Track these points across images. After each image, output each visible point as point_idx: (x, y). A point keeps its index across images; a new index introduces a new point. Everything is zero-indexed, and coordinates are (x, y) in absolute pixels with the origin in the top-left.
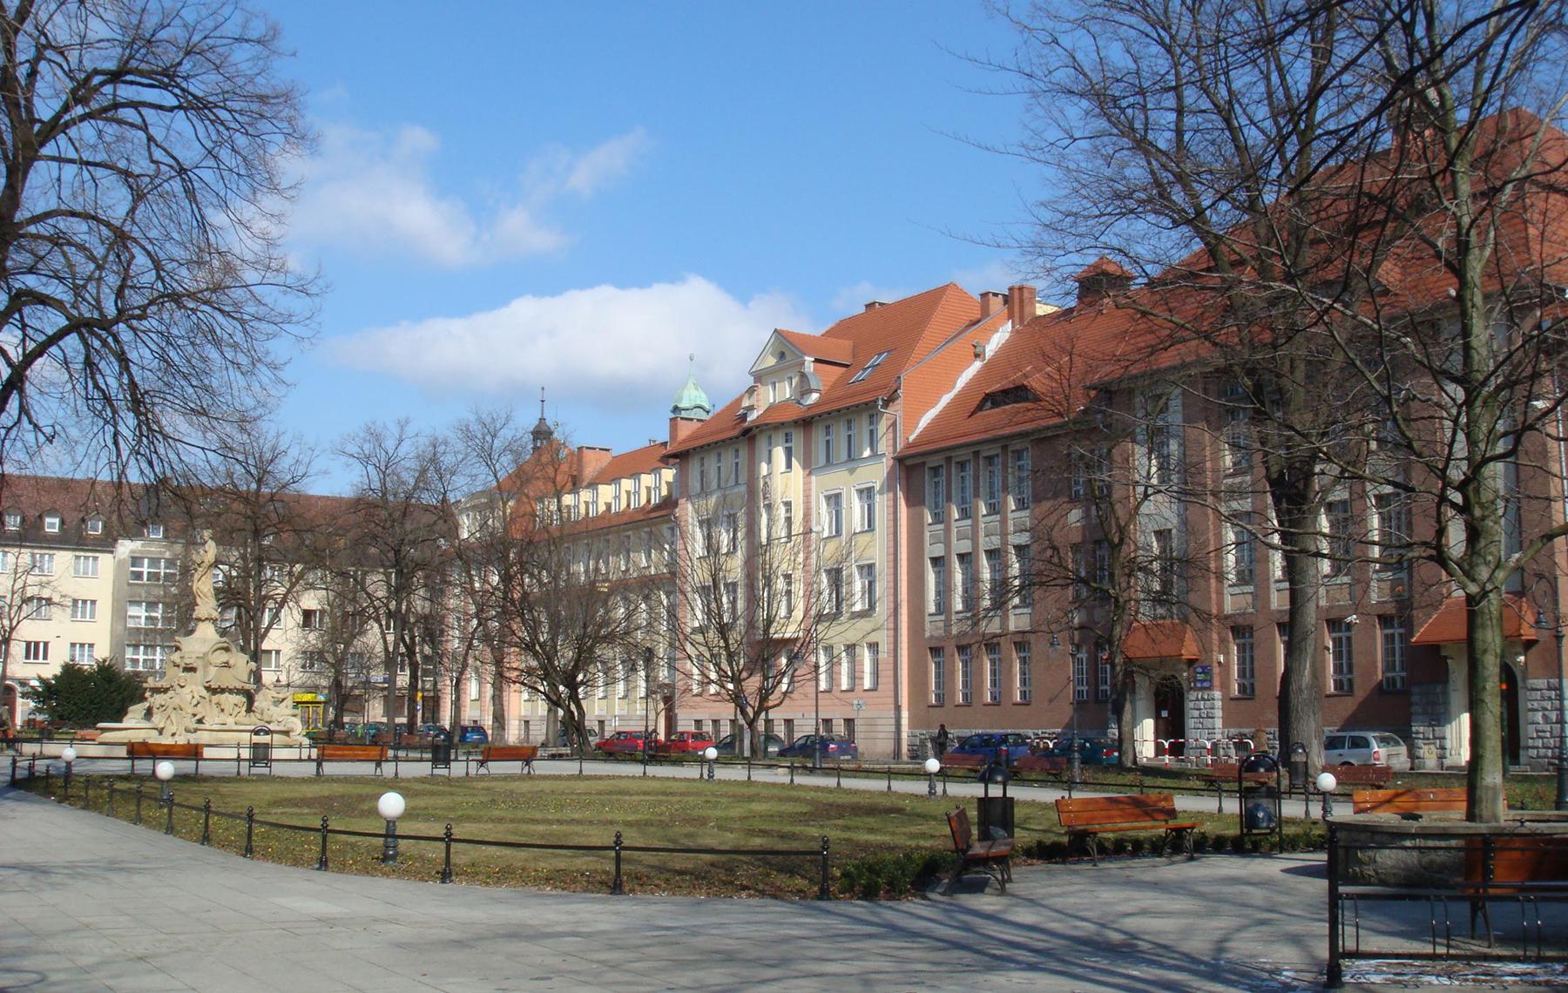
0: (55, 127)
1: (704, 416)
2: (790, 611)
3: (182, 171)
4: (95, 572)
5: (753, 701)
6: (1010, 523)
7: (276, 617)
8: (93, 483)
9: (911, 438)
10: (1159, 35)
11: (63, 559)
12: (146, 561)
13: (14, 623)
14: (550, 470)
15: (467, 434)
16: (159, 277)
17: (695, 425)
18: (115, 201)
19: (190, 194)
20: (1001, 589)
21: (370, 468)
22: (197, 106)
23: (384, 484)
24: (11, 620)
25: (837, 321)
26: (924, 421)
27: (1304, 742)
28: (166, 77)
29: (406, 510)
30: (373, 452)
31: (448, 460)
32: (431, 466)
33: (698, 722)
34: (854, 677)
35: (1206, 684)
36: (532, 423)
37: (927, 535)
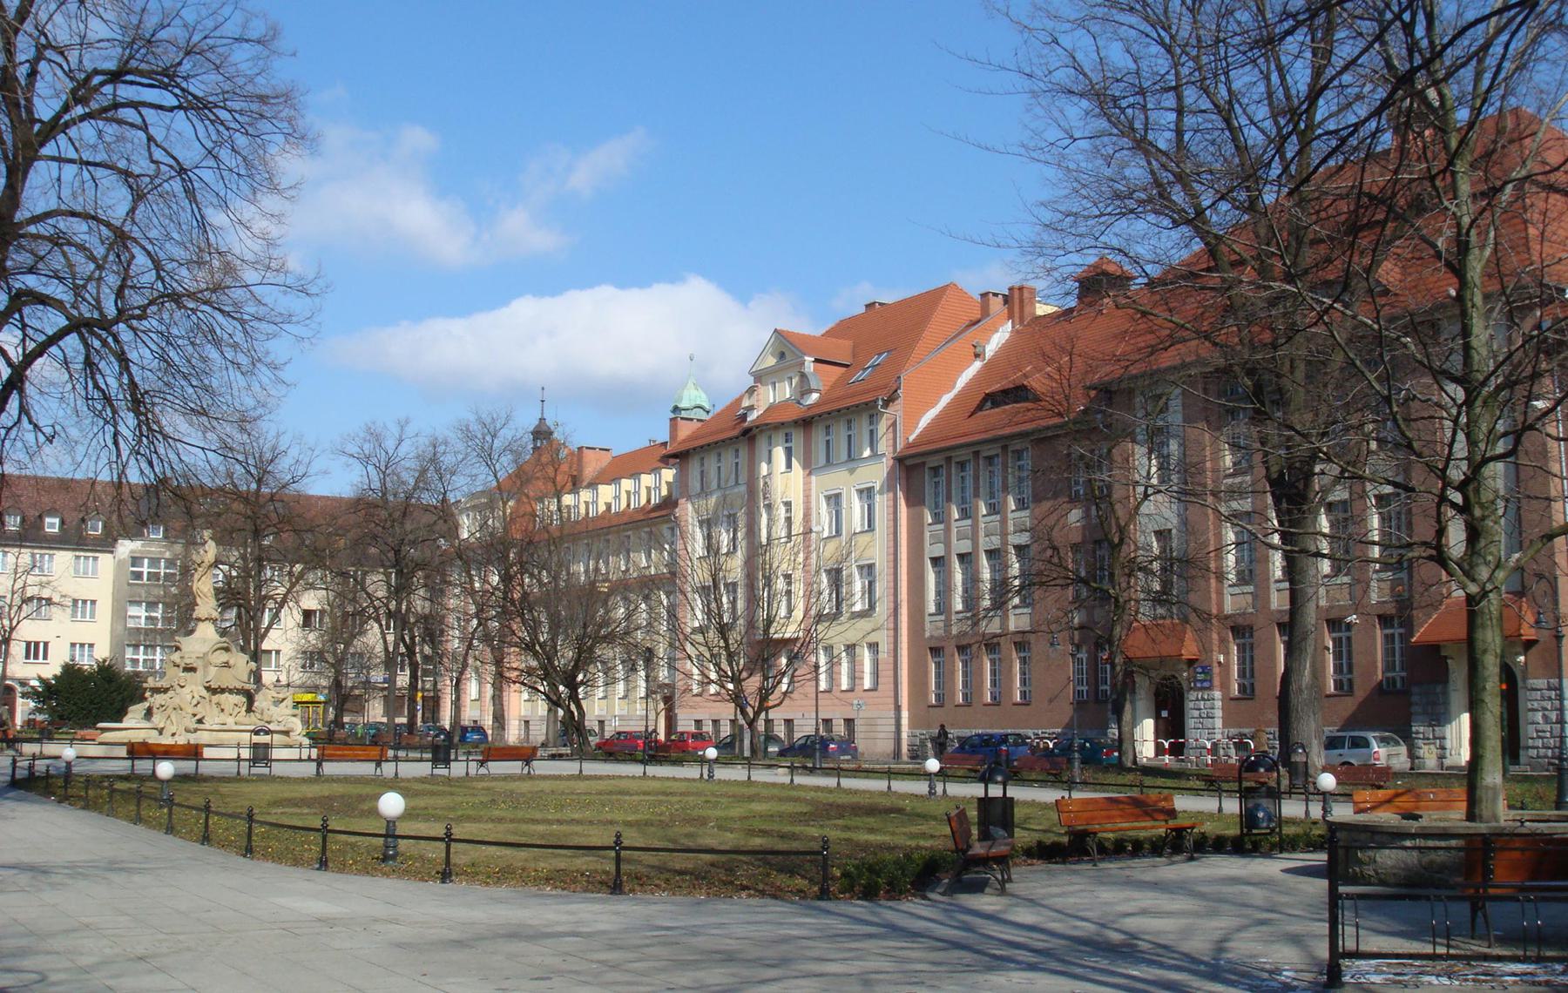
0: (55, 127)
1: (704, 416)
2: (790, 611)
3: (182, 171)
4: (95, 572)
5: (753, 701)
6: (1010, 523)
7: (276, 617)
8: (93, 483)
9: (911, 438)
10: (1159, 35)
11: (63, 559)
12: (146, 561)
13: (14, 623)
14: (550, 470)
15: (467, 434)
16: (159, 277)
17: (695, 425)
18: (115, 201)
19: (190, 194)
20: (1001, 589)
21: (370, 468)
22: (197, 106)
23: (384, 484)
24: (11, 620)
25: (837, 321)
26: (924, 421)
27: (1304, 742)
28: (166, 77)
29: (406, 510)
30: (373, 452)
31: (448, 460)
32: (431, 466)
34: (854, 677)
35: (1206, 684)
36: (532, 423)
37: (927, 535)
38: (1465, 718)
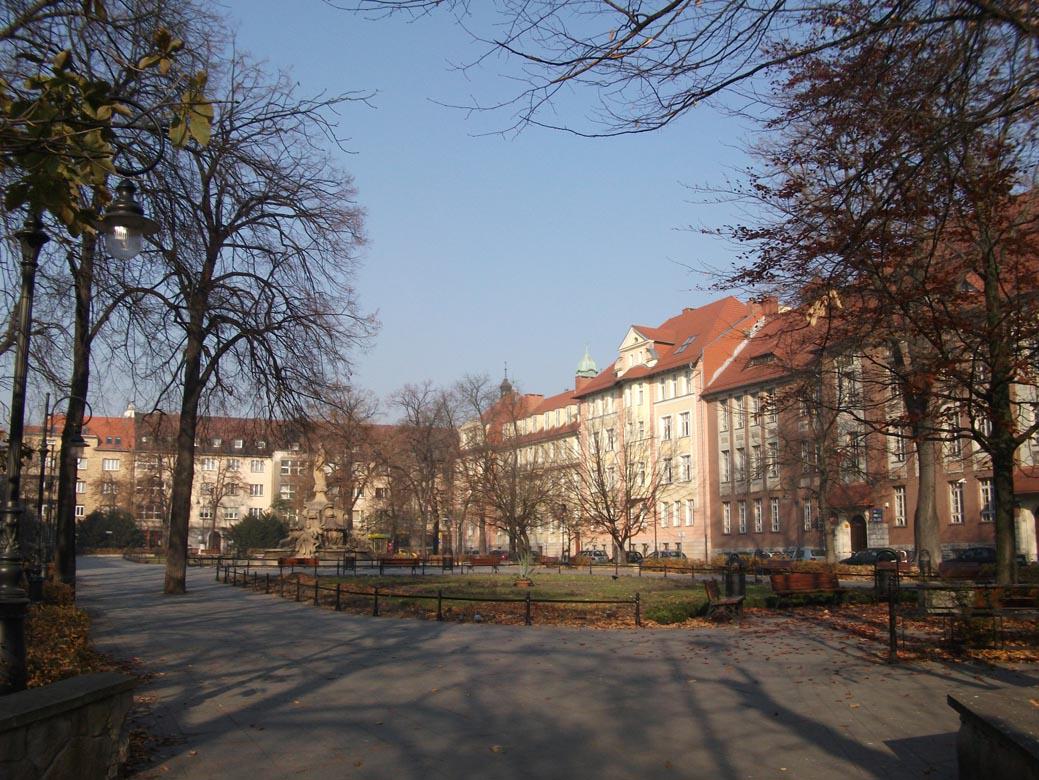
0: (233, 228)
1: (594, 375)
2: (643, 482)
3: (299, 251)
5: (622, 533)
6: (735, 436)
7: (361, 492)
8: (246, 420)
9: (709, 384)
10: (271, 291)
14: (510, 408)
15: (463, 389)
16: (288, 308)
17: (589, 381)
18: (263, 271)
19: (304, 266)
20: (764, 468)
21: (410, 409)
22: (304, 214)
23: (417, 418)
25: (667, 319)
26: (716, 375)
27: (929, 550)
28: (290, 202)
29: (429, 430)
30: (410, 398)
31: (451, 404)
32: (442, 406)
34: (682, 520)
35: (879, 520)
36: (499, 382)
37: (720, 439)
38: (46, 473)
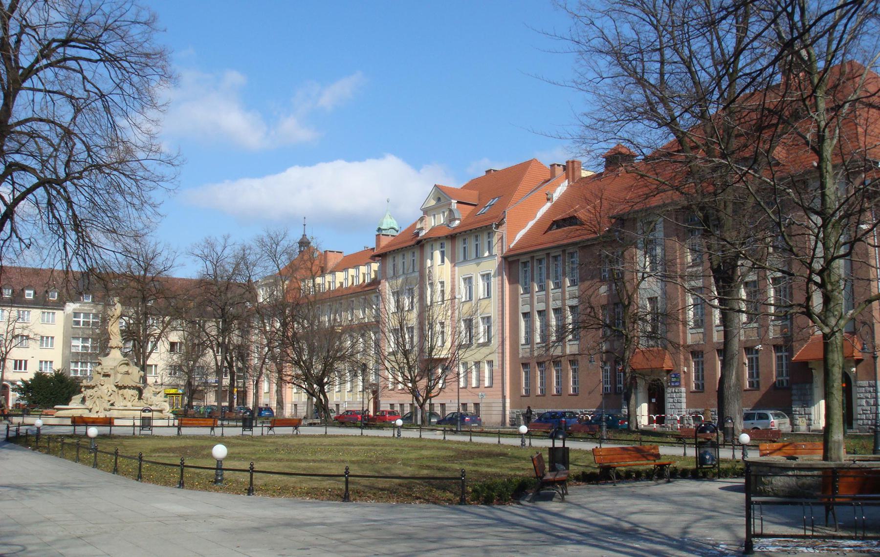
0: (31, 71)
1: (395, 233)
2: (443, 343)
3: (102, 96)
4: (53, 321)
5: (423, 393)
6: (567, 294)
7: (155, 346)
8: (52, 271)
9: (511, 246)
10: (651, 20)
11: (35, 314)
12: (82, 315)
13: (8, 349)
14: (309, 264)
15: (262, 244)
16: (89, 155)
17: (390, 238)
18: (65, 113)
19: (107, 109)
20: (562, 330)
21: (208, 262)
22: (110, 59)
23: (215, 271)
24: (6, 348)
25: (470, 180)
26: (519, 236)
27: (732, 416)
28: (93, 43)
29: (228, 286)
30: (209, 254)
31: (251, 258)
32: (242, 261)
33: (392, 405)
34: (480, 380)
35: (677, 384)
36: (299, 237)
37: (520, 300)
38: (822, 403)
